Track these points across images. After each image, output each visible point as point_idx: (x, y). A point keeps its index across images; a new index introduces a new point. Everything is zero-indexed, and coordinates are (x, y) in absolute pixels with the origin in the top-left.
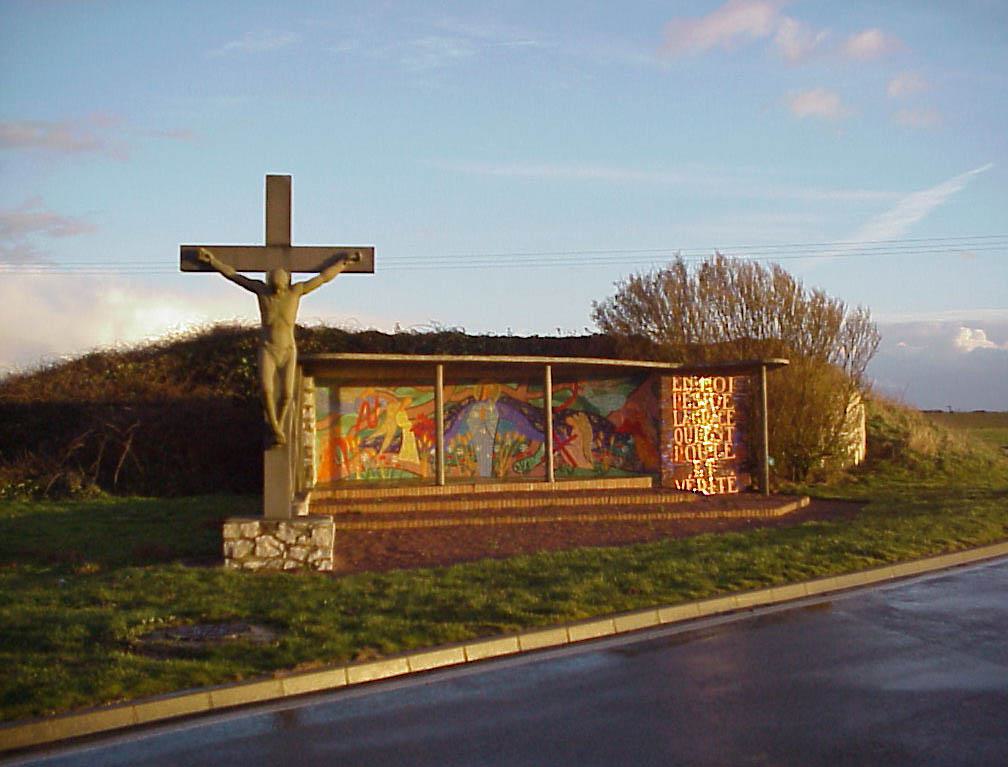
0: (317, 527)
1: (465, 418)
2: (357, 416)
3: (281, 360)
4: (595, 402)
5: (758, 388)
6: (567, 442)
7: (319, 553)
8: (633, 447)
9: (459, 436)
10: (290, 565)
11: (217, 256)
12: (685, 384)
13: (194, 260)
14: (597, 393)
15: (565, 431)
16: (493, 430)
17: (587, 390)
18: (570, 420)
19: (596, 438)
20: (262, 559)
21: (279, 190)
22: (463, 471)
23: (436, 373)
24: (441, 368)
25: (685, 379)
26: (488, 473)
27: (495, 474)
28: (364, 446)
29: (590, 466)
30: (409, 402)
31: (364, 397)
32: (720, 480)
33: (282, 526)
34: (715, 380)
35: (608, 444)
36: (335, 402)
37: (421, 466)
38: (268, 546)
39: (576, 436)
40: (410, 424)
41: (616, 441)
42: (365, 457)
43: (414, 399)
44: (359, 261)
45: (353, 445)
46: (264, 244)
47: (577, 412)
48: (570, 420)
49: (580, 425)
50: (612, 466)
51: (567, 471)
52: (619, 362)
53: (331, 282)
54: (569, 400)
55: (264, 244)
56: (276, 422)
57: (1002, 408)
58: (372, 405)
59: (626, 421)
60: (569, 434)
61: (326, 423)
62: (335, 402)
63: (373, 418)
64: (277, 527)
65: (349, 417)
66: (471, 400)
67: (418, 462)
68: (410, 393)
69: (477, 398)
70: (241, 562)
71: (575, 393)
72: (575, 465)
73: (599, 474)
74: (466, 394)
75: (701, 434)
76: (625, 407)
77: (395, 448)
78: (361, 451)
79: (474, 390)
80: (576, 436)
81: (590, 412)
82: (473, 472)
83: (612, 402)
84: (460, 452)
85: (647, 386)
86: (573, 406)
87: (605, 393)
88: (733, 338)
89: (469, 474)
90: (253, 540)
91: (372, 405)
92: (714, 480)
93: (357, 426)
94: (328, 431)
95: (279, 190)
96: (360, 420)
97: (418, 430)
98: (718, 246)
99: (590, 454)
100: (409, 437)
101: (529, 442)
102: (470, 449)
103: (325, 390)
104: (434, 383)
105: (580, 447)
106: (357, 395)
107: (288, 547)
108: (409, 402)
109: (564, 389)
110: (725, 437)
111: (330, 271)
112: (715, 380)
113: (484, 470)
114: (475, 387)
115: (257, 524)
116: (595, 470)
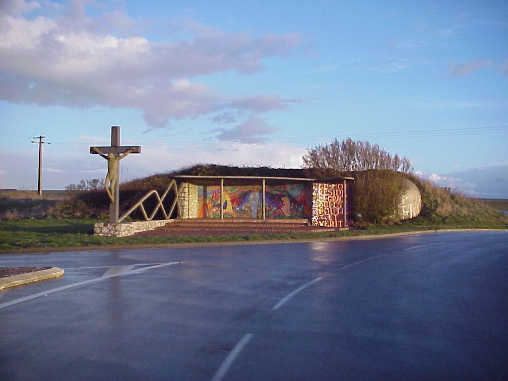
0: (117, 225)
1: (249, 197)
2: (211, 196)
3: (111, 178)
4: (291, 192)
5: (151, 188)
6: (281, 206)
7: (117, 233)
8: (303, 209)
9: (246, 204)
10: (110, 235)
11: (99, 150)
12: (325, 187)
13: (93, 151)
14: (292, 189)
15: (281, 202)
16: (257, 202)
17: (288, 188)
18: (282, 199)
19: (291, 205)
20: (103, 233)
21: (115, 131)
22: (247, 215)
23: (262, 182)
24: (222, 180)
25: (325, 184)
26: (256, 217)
27: (258, 217)
28: (214, 206)
29: (288, 215)
30: (229, 192)
31: (214, 190)
32: (340, 222)
33: (109, 224)
34: (339, 185)
35: (295, 208)
36: (205, 191)
37: (233, 214)
38: (105, 230)
39: (284, 204)
40: (230, 199)
41: (298, 206)
42: (214, 210)
43: (231, 191)
44: (136, 150)
45: (210, 206)
46: (110, 146)
47: (285, 196)
48: (282, 199)
49: (286, 201)
50: (296, 215)
51: (282, 216)
52: (272, 178)
53: (127, 156)
54: (282, 192)
55: (110, 146)
56: (159, 199)
57: (504, 196)
58: (217, 193)
59: (301, 200)
60: (282, 203)
61: (202, 198)
62: (205, 191)
63: (217, 197)
64: (107, 225)
65: (210, 196)
66: (250, 191)
67: (232, 212)
68: (230, 188)
69: (252, 190)
70: (98, 234)
71: (284, 189)
72: (284, 214)
73: (291, 218)
74: (249, 189)
75: (332, 205)
76: (301, 194)
77: (225, 207)
78: (213, 208)
79: (250, 187)
80: (284, 204)
81: (290, 196)
82: (251, 216)
83: (296, 192)
84: (246, 209)
85: (308, 188)
86: (284, 193)
87: (294, 189)
88: (357, 170)
89: (249, 216)
90: (101, 228)
91: (217, 193)
92: (337, 222)
93: (212, 199)
94: (202, 201)
95: (115, 131)
96: (213, 197)
97: (232, 201)
98: (347, 134)
99: (289, 211)
100: (229, 203)
101: (269, 206)
102: (250, 208)
103: (202, 187)
104: (220, 185)
105: (286, 209)
106: (212, 189)
107: (110, 230)
108: (229, 192)
109: (281, 187)
110: (343, 206)
111: (126, 153)
112: (339, 185)
113: (255, 216)
114: (252, 186)
115: (103, 224)
116: (290, 216)
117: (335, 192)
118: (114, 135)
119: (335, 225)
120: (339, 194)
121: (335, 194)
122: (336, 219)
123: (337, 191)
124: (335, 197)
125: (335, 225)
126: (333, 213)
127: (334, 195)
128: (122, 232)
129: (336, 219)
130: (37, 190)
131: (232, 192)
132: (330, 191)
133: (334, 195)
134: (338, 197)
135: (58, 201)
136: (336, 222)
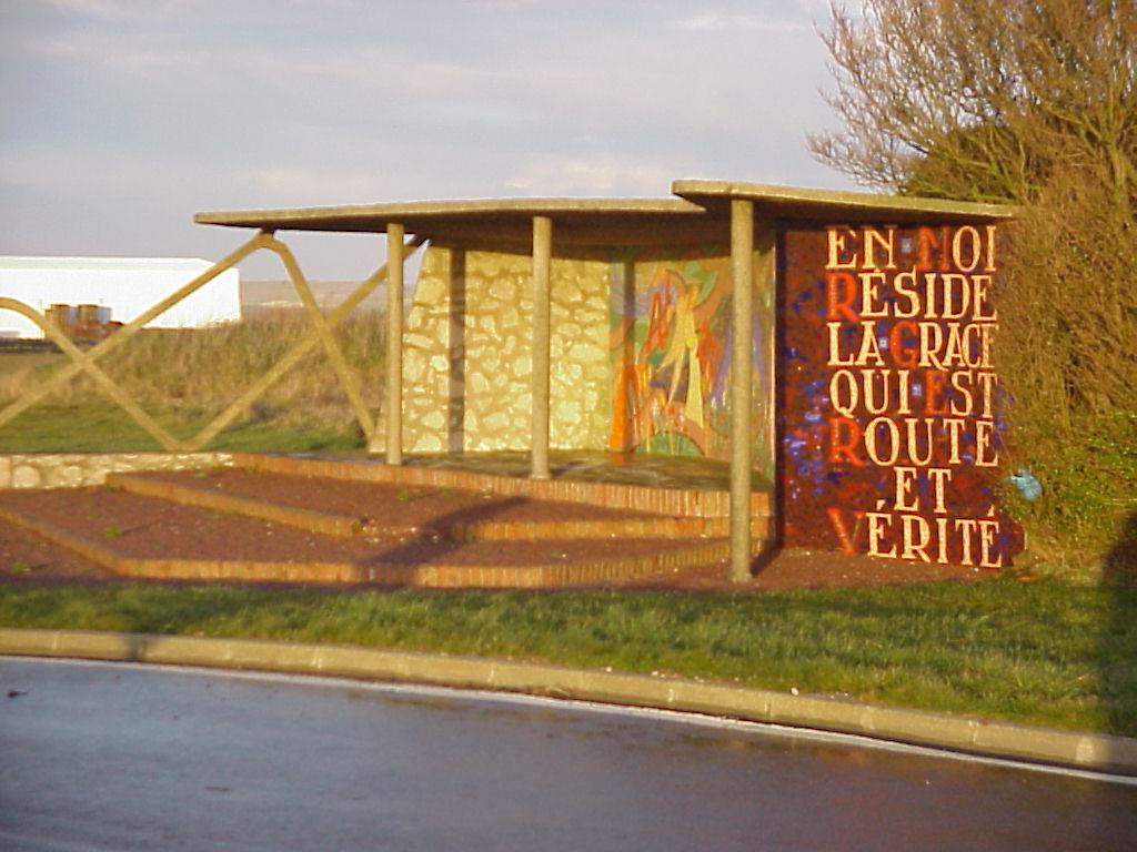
13: (201, 220)
34: (958, 236)
117: (939, 284)
118: (147, 318)
119: (933, 550)
120: (956, 309)
121: (939, 308)
122: (940, 508)
123: (947, 278)
124: (939, 335)
125: (933, 550)
126: (922, 455)
127: (931, 314)
128: (1010, 608)
129: (940, 508)
130: (286, 275)
131: (706, 292)
132: (907, 284)
133: (931, 314)
134: (954, 327)
135: (270, 387)
136: (942, 522)
